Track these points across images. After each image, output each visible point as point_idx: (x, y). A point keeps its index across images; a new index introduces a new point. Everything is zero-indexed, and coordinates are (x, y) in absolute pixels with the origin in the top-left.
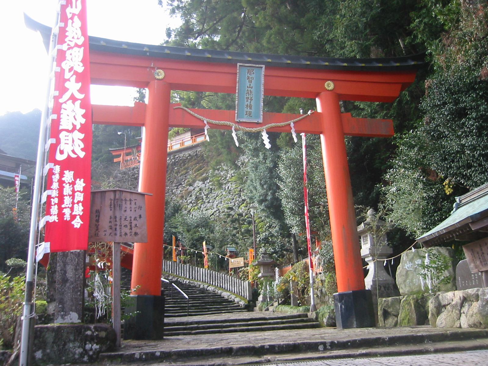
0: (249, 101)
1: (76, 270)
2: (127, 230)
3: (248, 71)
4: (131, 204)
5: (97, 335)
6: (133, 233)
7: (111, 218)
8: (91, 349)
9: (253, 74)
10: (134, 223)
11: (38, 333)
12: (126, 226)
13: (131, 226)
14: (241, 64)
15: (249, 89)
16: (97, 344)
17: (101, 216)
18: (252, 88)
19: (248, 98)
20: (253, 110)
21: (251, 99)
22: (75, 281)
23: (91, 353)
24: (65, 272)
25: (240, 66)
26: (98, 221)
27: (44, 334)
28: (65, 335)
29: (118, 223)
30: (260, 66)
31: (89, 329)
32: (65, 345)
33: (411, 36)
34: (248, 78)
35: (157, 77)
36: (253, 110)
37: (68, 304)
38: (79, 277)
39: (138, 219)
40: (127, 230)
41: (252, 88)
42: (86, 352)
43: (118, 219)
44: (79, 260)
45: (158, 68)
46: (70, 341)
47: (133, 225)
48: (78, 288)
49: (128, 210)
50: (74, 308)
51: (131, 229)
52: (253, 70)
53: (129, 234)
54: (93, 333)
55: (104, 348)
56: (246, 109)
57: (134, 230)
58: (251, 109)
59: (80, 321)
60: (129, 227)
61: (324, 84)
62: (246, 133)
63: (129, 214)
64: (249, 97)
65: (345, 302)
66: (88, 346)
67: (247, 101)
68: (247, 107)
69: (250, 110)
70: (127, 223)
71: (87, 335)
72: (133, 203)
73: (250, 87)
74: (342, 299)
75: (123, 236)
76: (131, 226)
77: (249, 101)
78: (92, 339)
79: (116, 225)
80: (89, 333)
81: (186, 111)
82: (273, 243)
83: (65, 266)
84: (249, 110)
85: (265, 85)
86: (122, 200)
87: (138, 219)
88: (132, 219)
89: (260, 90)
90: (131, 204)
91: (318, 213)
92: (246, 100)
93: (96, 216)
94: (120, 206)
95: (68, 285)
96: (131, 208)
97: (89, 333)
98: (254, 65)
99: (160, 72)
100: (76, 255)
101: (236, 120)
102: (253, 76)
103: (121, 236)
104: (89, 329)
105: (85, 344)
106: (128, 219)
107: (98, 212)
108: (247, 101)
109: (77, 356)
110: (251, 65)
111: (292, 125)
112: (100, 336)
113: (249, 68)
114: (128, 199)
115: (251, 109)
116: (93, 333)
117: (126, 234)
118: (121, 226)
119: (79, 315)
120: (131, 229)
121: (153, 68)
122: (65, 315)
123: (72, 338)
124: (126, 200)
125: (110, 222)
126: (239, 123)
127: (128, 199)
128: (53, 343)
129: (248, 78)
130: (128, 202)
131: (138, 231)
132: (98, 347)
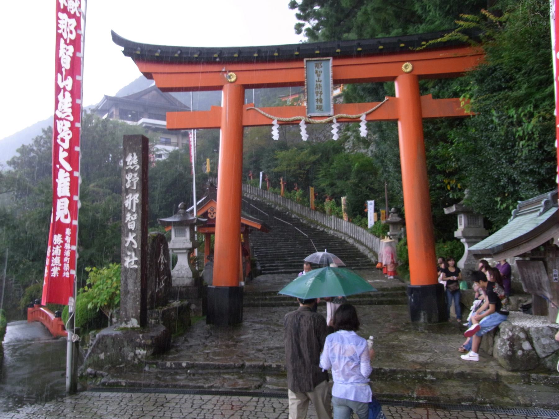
1: (135, 283)
8: (140, 354)
9: (321, 67)
14: (308, 59)
15: (318, 83)
19: (317, 93)
21: (321, 93)
22: (135, 292)
23: (140, 357)
24: (127, 285)
25: (307, 61)
30: (328, 58)
33: (118, 259)
35: (230, 80)
38: (137, 289)
42: (136, 355)
44: (137, 274)
45: (230, 71)
56: (316, 104)
59: (139, 326)
61: (401, 69)
65: (414, 296)
66: (138, 351)
67: (317, 95)
74: (412, 293)
77: (319, 95)
78: (141, 346)
80: (138, 340)
81: (259, 112)
83: (126, 279)
84: (319, 104)
85: (334, 76)
89: (329, 82)
91: (492, 142)
92: (315, 95)
95: (129, 296)
98: (321, 59)
102: (321, 69)
105: (135, 349)
108: (317, 95)
110: (318, 59)
111: (363, 118)
113: (316, 62)
116: (141, 340)
129: (317, 72)
132: (145, 352)
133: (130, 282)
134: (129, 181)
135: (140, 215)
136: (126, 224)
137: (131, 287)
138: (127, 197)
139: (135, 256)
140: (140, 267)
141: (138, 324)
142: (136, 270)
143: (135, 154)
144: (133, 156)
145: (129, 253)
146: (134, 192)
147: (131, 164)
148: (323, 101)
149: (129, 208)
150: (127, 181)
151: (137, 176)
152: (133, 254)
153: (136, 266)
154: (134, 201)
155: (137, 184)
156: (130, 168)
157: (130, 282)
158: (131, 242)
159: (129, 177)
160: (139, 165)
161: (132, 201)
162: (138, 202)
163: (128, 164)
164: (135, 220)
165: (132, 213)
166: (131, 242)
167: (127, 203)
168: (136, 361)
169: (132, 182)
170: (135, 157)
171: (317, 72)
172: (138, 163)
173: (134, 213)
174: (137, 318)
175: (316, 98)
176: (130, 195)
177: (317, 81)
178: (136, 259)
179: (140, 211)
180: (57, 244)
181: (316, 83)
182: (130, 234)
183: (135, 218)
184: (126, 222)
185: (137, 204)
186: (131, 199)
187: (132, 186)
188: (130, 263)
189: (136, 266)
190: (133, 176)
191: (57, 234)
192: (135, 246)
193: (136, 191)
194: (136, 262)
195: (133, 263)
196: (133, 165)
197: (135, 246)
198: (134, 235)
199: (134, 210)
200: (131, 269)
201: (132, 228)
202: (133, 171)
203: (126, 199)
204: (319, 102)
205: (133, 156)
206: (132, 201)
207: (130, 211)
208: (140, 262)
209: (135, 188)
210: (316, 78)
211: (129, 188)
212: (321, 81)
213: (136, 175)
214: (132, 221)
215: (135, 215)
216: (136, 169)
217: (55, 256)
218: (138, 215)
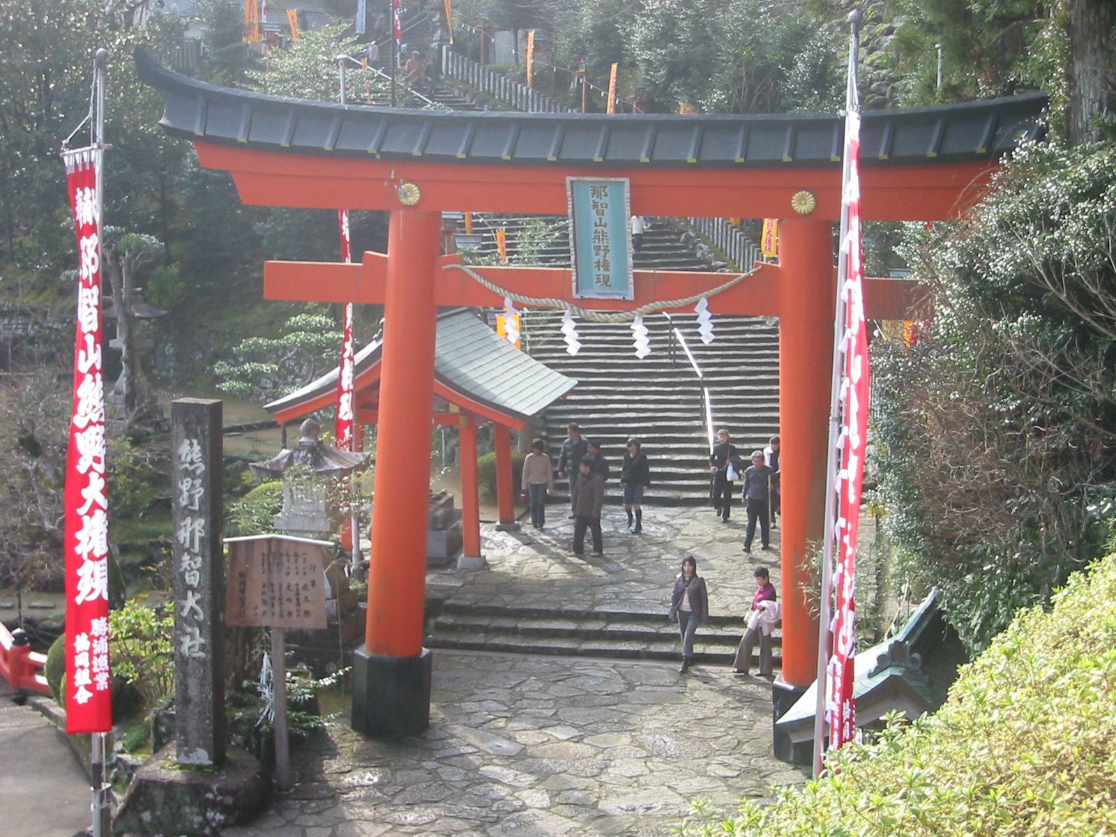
0: (602, 253)
1: (202, 685)
2: (292, 607)
3: (594, 190)
4: (296, 561)
5: (221, 801)
6: (302, 613)
7: (264, 586)
8: (214, 820)
10: (303, 594)
11: (143, 788)
12: (290, 600)
13: (298, 599)
15: (600, 229)
16: (221, 814)
17: (249, 583)
18: (605, 226)
20: (611, 273)
21: (606, 250)
23: (214, 824)
24: (187, 688)
26: (243, 591)
27: (150, 790)
28: (178, 795)
29: (277, 594)
31: (210, 790)
32: (179, 808)
34: (595, 205)
35: (404, 201)
36: (611, 273)
37: (193, 736)
39: (310, 587)
40: (292, 607)
41: (605, 226)
43: (276, 588)
44: (204, 671)
45: (407, 181)
46: (186, 804)
47: (302, 599)
48: (205, 713)
49: (293, 571)
50: (201, 742)
51: (298, 604)
52: (605, 188)
53: (295, 614)
54: (216, 797)
55: (231, 820)
56: (595, 271)
57: (304, 606)
58: (606, 269)
59: (211, 763)
60: (294, 601)
62: (829, 57)
63: (293, 580)
64: (601, 244)
66: (210, 814)
68: (598, 266)
69: (607, 273)
70: (292, 595)
71: (208, 799)
72: (300, 560)
73: (600, 225)
75: (286, 617)
76: (298, 599)
78: (214, 805)
79: (273, 598)
80: (210, 796)
82: (1024, 229)
84: (602, 272)
86: (281, 555)
87: (310, 587)
88: (300, 588)
90: (296, 561)
92: (594, 252)
93: (241, 583)
94: (280, 564)
95: (191, 707)
96: (297, 568)
97: (210, 796)
99: (410, 190)
100: (200, 662)
101: (575, 295)
102: (606, 200)
103: (282, 616)
104: (210, 790)
105: (206, 811)
106: (293, 588)
107: (242, 575)
108: (597, 254)
109: (196, 826)
112: (225, 802)
114: (292, 553)
115: (606, 269)
117: (290, 614)
118: (281, 599)
119: (209, 754)
120: (298, 604)
121: (396, 181)
122: (191, 752)
123: (188, 799)
124: (288, 555)
125: (263, 593)
126: (584, 303)
127: (292, 553)
128: (164, 803)
130: (293, 559)
131: (310, 607)
132: (222, 817)
133: (193, 683)
134: (186, 494)
135: (208, 559)
136: (182, 575)
137: (193, 692)
138: (183, 524)
139: (200, 635)
140: (209, 656)
141: (209, 759)
142: (202, 662)
143: (195, 441)
144: (191, 445)
145: (189, 630)
146: (193, 514)
147: (189, 459)
148: (611, 268)
149: (187, 545)
150: (181, 492)
151: (201, 486)
152: (197, 631)
153: (202, 655)
154: (197, 531)
155: (202, 501)
156: (186, 469)
157: (193, 683)
158: (191, 608)
159: (185, 485)
160: (205, 464)
161: (192, 533)
162: (203, 535)
163: (183, 458)
164: (198, 570)
165: (193, 556)
166: (191, 608)
167: (183, 535)
168: (207, 831)
169: (191, 497)
170: (197, 448)
171: (595, 205)
172: (203, 460)
173: (197, 555)
174: (205, 747)
175: (595, 259)
176: (189, 520)
177: (596, 225)
178: (203, 641)
179: (208, 553)
180: (100, 636)
181: (594, 228)
182: (190, 593)
183: (199, 565)
184: (182, 570)
185: (202, 539)
186: (189, 529)
187: (192, 504)
188: (190, 648)
189: (202, 655)
190: (193, 485)
191: (99, 618)
192: (201, 617)
193: (199, 514)
194: (203, 648)
195: (197, 647)
196: (192, 463)
197: (201, 617)
198: (198, 596)
199: (197, 549)
200: (194, 658)
201: (192, 582)
202: (191, 474)
203: (181, 528)
204: (602, 269)
205: (191, 445)
206: (192, 533)
207: (188, 551)
208: (209, 647)
209: (196, 507)
210: (595, 218)
211: (186, 506)
212: (605, 226)
213: (198, 482)
214: (192, 570)
215: (199, 559)
216: (198, 472)
217: (98, 656)
218: (204, 561)
